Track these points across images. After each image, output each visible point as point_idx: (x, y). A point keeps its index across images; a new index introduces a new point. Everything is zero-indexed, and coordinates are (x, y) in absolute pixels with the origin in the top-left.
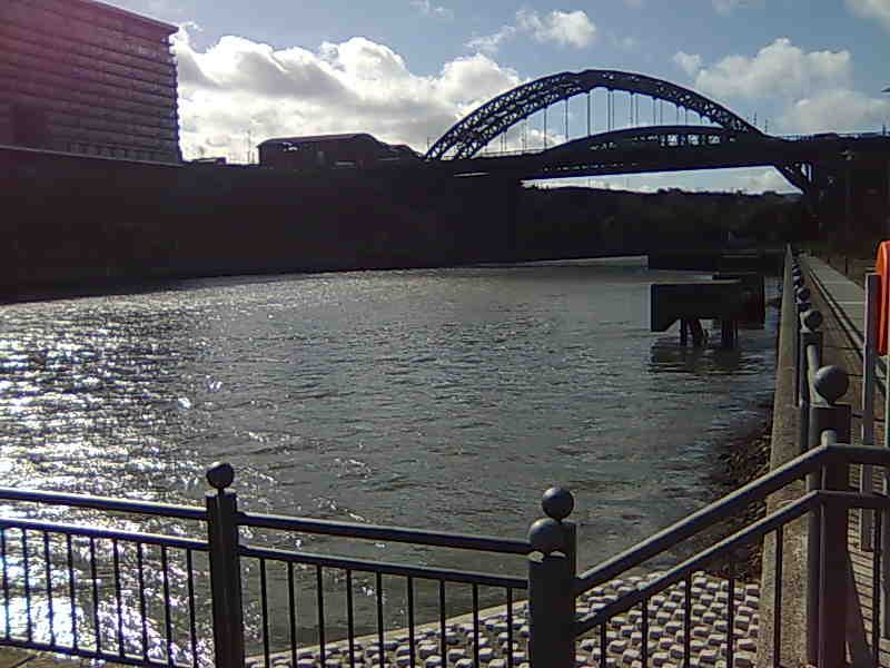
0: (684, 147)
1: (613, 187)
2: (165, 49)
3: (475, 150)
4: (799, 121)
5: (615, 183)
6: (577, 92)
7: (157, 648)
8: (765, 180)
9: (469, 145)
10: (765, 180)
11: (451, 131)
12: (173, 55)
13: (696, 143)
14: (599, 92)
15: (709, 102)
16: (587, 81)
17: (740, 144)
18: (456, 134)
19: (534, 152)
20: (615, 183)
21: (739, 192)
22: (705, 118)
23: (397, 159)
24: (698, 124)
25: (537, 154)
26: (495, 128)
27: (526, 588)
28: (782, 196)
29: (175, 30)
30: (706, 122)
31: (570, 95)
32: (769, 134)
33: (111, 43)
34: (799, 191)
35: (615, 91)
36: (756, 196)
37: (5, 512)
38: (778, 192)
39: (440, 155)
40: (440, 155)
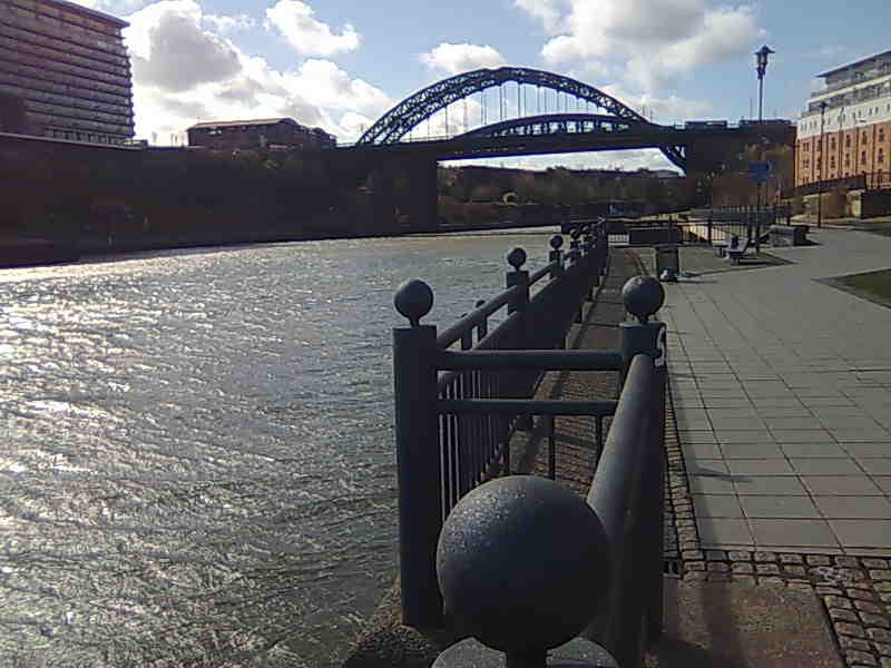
0: (546, 135)
1: (506, 166)
2: (117, 42)
3: (401, 135)
4: (673, 112)
5: (511, 163)
6: (491, 85)
7: (564, 237)
8: (653, 159)
9: (396, 130)
10: (653, 159)
11: (383, 119)
12: (126, 48)
13: (522, 133)
14: (511, 85)
15: (584, 86)
16: (501, 76)
17: (630, 130)
18: (386, 121)
19: (348, 145)
20: (511, 163)
21: (617, 169)
22: (600, 108)
23: (285, 147)
24: (595, 112)
25: (351, 147)
26: (419, 116)
27: (463, 349)
28: (652, 172)
29: (127, 25)
30: (603, 112)
31: (486, 87)
32: (654, 122)
33: (76, 38)
34: (681, 172)
35: (524, 85)
36: (632, 173)
37: (3, 372)
38: (651, 169)
39: (372, 140)
40: (372, 140)
